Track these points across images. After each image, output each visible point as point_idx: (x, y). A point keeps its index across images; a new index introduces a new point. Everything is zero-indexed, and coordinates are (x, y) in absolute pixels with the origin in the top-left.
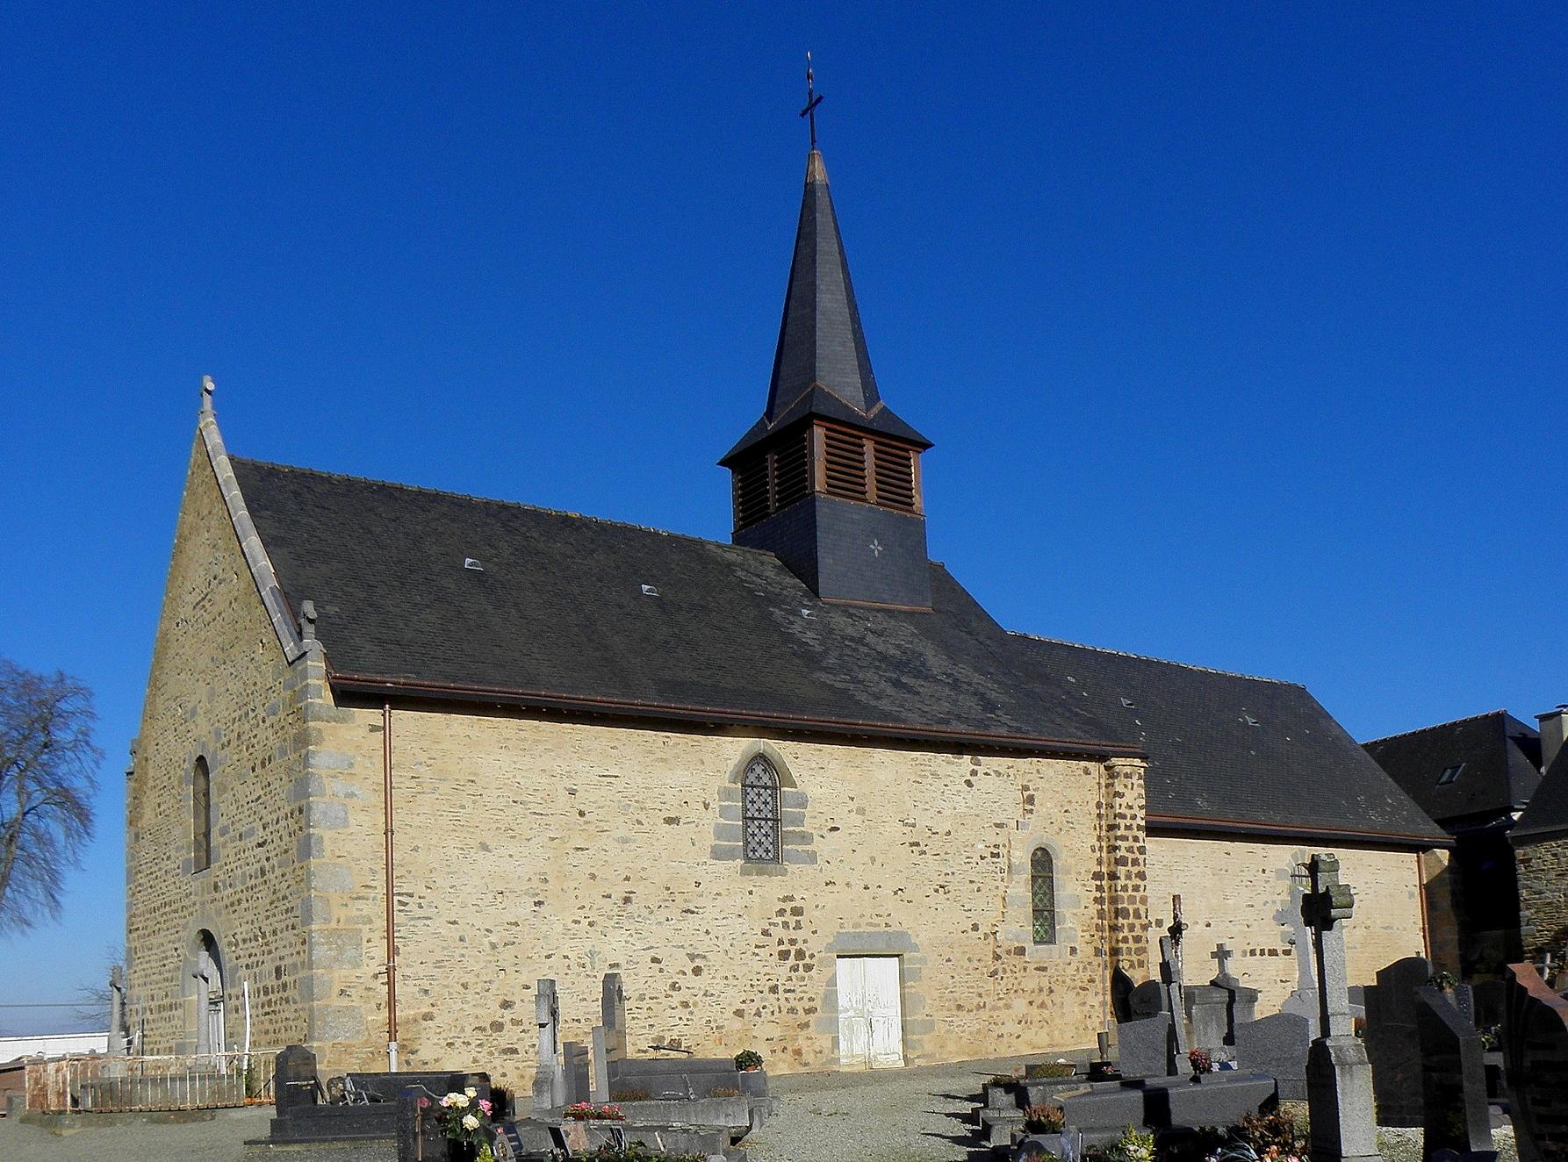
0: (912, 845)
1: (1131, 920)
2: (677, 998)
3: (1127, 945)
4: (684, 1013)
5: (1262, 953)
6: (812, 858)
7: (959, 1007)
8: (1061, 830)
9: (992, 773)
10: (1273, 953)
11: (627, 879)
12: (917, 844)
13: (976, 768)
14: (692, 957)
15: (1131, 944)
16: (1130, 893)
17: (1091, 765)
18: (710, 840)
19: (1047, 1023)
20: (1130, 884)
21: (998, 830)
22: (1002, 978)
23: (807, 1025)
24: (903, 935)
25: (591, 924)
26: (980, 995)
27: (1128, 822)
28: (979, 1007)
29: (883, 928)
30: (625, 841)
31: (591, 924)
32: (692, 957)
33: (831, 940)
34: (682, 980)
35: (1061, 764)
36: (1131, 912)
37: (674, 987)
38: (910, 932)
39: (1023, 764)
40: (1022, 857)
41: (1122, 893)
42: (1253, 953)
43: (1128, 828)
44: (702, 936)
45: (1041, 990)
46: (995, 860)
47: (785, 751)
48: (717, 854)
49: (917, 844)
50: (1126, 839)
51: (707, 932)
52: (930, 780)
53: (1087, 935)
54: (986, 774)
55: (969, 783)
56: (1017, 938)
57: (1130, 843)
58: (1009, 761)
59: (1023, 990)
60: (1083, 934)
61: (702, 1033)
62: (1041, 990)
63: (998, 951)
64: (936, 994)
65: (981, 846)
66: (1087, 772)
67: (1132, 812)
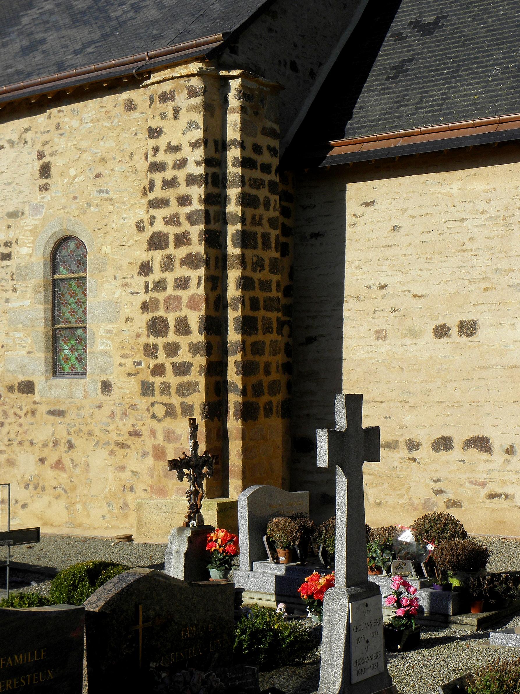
1: (172, 337)
8: (89, 205)
19: (65, 491)
20: (170, 277)
21: (11, 221)
27: (169, 174)
36: (172, 324)
43: (169, 184)
45: (56, 443)
53: (129, 362)
56: (22, 368)
57: (174, 208)
59: (32, 443)
60: (123, 361)
62: (56, 443)
66: (130, 106)
67: (179, 156)
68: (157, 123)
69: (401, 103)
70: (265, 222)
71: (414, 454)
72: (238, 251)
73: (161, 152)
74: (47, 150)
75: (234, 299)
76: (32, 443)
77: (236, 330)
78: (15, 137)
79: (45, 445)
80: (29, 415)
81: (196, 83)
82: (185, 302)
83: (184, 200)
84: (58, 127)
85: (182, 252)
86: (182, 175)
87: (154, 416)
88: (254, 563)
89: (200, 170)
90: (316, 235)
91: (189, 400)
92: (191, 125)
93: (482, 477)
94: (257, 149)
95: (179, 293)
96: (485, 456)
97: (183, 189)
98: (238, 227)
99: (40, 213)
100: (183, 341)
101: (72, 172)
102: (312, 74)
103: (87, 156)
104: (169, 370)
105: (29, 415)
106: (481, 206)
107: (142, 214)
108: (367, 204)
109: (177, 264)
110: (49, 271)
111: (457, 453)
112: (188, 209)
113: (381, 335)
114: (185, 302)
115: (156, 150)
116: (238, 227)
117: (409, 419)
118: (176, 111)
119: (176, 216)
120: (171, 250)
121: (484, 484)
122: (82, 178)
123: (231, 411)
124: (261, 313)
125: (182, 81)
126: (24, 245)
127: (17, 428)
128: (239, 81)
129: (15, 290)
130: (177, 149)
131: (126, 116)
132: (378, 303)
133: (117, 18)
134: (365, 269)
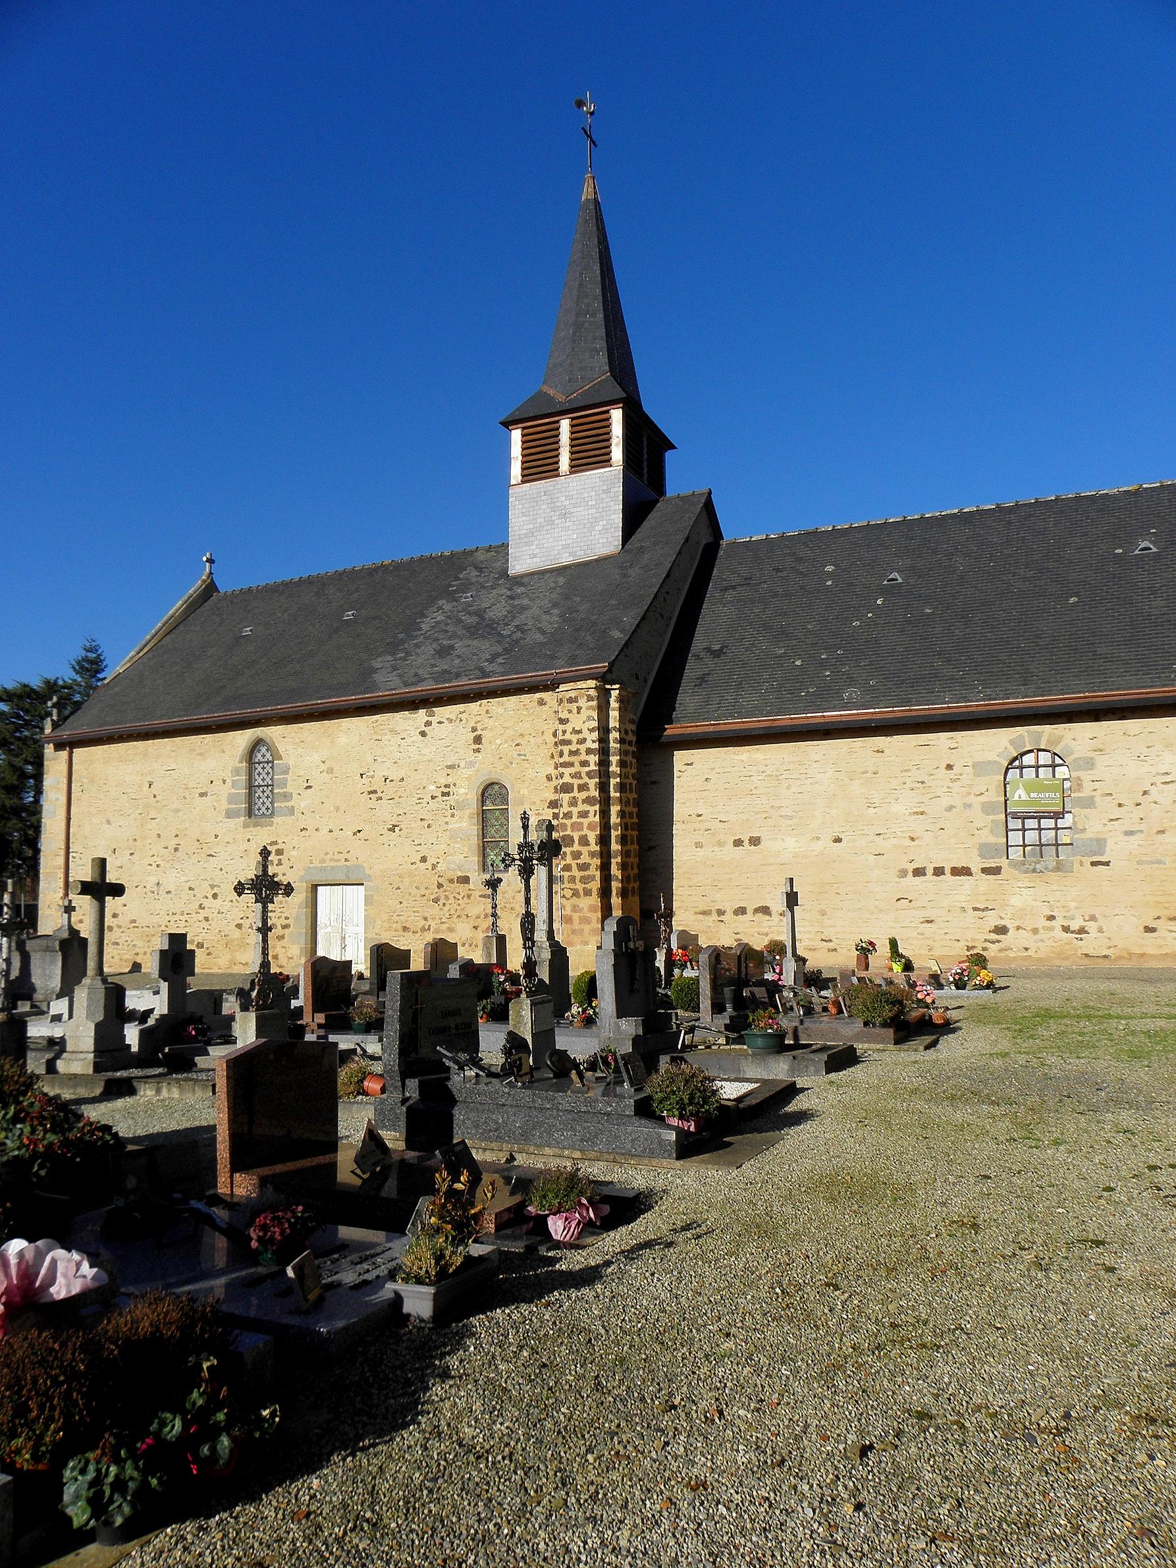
0: (370, 793)
2: (203, 913)
3: (569, 874)
4: (205, 924)
5: (939, 872)
6: (291, 811)
7: (405, 929)
8: (511, 763)
9: (445, 721)
10: (964, 871)
11: (177, 836)
12: (375, 792)
13: (430, 719)
14: (212, 887)
15: (575, 872)
16: (575, 819)
17: (545, 695)
18: (225, 805)
20: (575, 810)
21: (449, 771)
22: (444, 904)
23: (283, 937)
24: (358, 867)
25: (158, 866)
26: (426, 919)
27: (574, 747)
28: (423, 929)
29: (343, 863)
30: (177, 811)
31: (158, 866)
32: (212, 887)
33: (302, 873)
34: (206, 903)
35: (512, 701)
37: (201, 907)
38: (365, 865)
39: (473, 707)
40: (467, 792)
41: (564, 821)
42: (919, 872)
43: (575, 753)
44: (219, 872)
46: (445, 798)
47: (273, 733)
48: (230, 815)
49: (375, 792)
50: (572, 765)
51: (221, 869)
52: (388, 737)
54: (440, 723)
55: (423, 734)
58: (461, 707)
59: (467, 916)
61: (216, 939)
63: (440, 880)
64: (385, 917)
65: (432, 787)
66: (541, 702)
67: (581, 736)
68: (564, 715)
69: (707, 702)
70: (630, 777)
71: (722, 918)
72: (618, 795)
73: (568, 734)
74: (479, 726)
75: (616, 824)
76: (467, 916)
77: (617, 843)
78: (453, 717)
79: (478, 917)
80: (465, 898)
81: (593, 693)
82: (585, 826)
83: (584, 764)
84: (487, 712)
85: (584, 795)
86: (583, 748)
87: (564, 896)
88: (407, 1081)
89: (596, 745)
90: (654, 783)
91: (588, 886)
92: (589, 718)
93: (767, 930)
94: (626, 732)
95: (582, 820)
96: (767, 917)
97: (583, 757)
98: (618, 780)
99: (474, 767)
100: (584, 850)
101: (498, 741)
102: (646, 681)
103: (510, 732)
104: (574, 867)
105: (465, 898)
106: (762, 768)
107: (551, 770)
108: (688, 764)
109: (580, 803)
110: (480, 804)
111: (749, 915)
112: (587, 769)
113: (698, 845)
114: (585, 826)
115: (564, 732)
116: (618, 780)
117: (718, 896)
118: (579, 709)
119: (580, 773)
120: (575, 793)
121: (767, 935)
122: (506, 745)
123: (614, 893)
124: (629, 832)
125: (583, 691)
126: (462, 787)
127: (456, 907)
128: (618, 691)
129: (453, 816)
130: (580, 732)
131: (539, 708)
132: (696, 826)
133: (509, 636)
134: (688, 804)
